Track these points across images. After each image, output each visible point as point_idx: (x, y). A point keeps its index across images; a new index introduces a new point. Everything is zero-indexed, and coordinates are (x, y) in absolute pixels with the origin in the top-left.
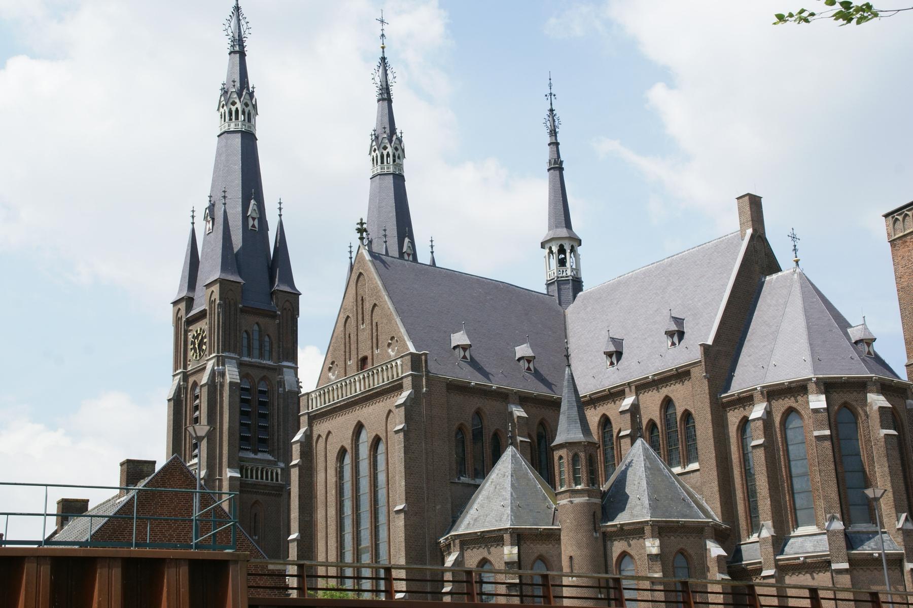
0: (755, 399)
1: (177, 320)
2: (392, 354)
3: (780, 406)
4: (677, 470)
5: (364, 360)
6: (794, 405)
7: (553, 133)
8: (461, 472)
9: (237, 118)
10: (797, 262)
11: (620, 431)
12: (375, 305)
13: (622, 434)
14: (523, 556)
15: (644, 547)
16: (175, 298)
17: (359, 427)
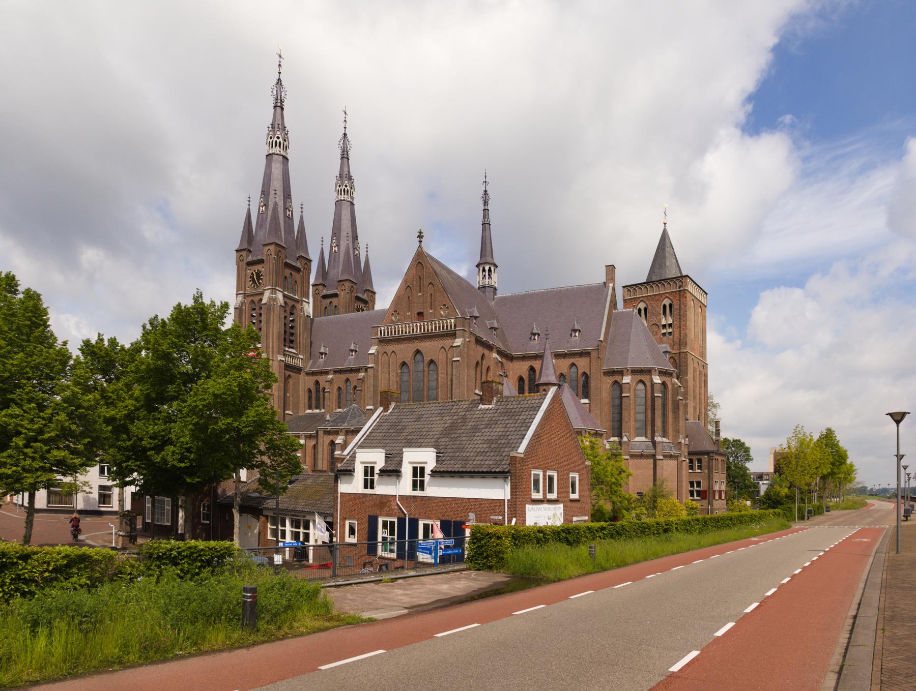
7: (486, 203)
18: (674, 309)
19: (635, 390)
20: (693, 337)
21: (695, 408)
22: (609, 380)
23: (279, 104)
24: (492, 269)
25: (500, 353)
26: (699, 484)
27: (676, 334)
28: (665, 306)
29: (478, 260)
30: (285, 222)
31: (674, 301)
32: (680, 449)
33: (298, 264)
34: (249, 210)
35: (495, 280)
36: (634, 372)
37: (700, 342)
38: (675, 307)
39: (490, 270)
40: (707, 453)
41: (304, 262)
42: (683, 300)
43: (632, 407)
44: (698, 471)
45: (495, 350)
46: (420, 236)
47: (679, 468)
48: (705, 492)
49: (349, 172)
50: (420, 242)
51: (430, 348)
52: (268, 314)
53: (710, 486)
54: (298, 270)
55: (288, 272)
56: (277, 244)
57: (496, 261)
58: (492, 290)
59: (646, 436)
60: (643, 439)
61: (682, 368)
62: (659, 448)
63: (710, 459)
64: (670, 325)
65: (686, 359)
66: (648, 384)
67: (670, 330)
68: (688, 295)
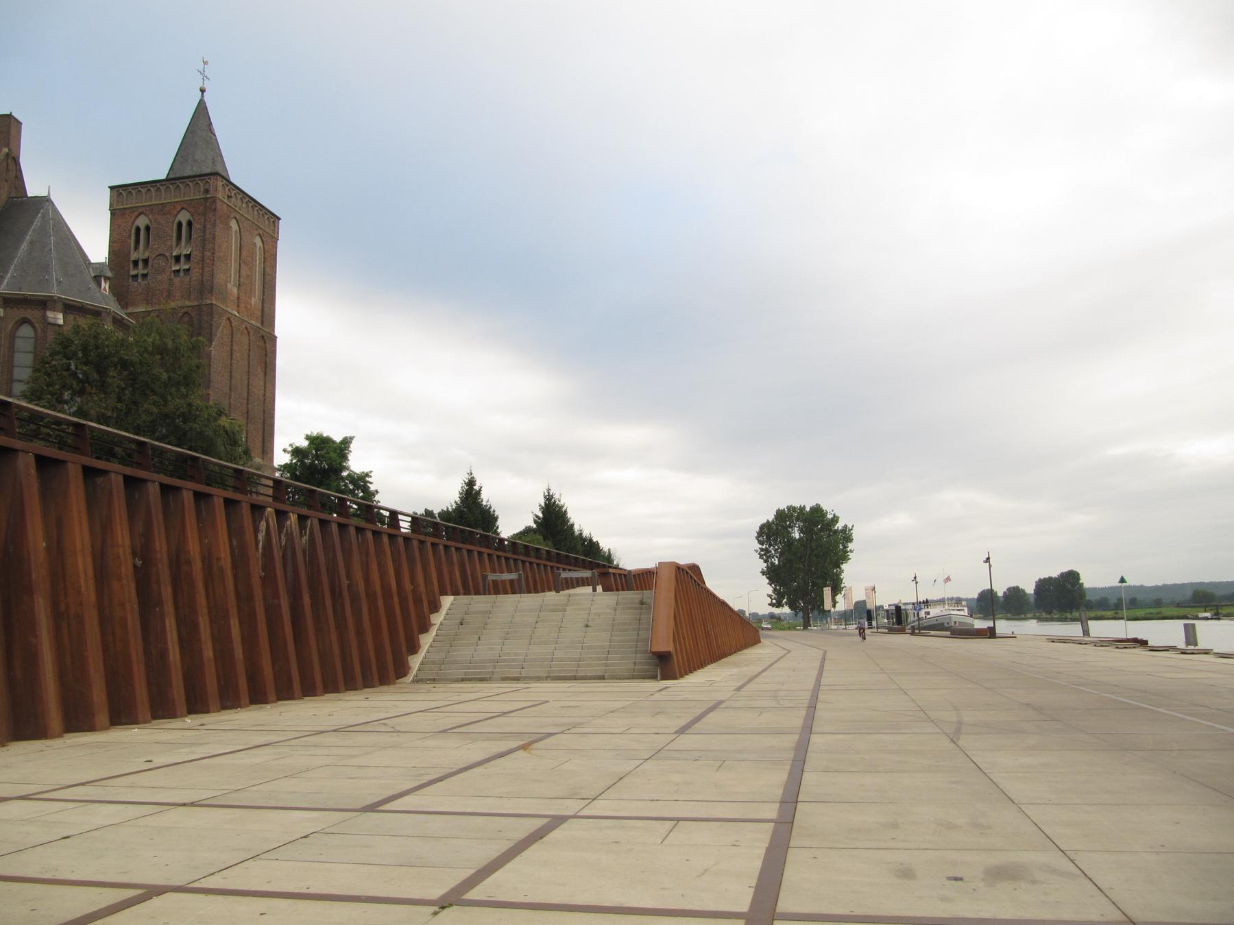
27: (195, 274)
28: (180, 224)
38: (196, 226)
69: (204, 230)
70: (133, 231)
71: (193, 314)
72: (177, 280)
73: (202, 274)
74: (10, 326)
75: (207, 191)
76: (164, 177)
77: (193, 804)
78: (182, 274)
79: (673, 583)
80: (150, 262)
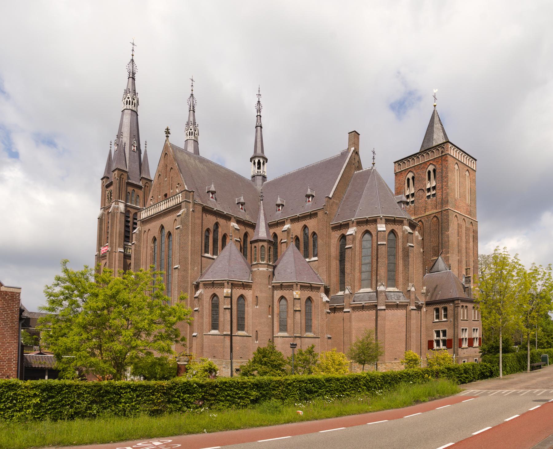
0: (350, 225)
1: (103, 185)
2: (177, 190)
3: (238, 292)
4: (307, 260)
5: (166, 195)
6: (369, 229)
7: (259, 111)
8: (207, 252)
9: (129, 104)
10: (374, 164)
11: (281, 240)
12: (172, 168)
13: (282, 241)
14: (233, 294)
15: (292, 295)
16: (102, 177)
17: (162, 227)
18: (437, 173)
19: (361, 241)
20: (457, 196)
21: (460, 262)
22: (336, 235)
23: (131, 76)
24: (262, 161)
25: (239, 222)
26: (444, 332)
27: (439, 195)
28: (429, 172)
29: (252, 154)
30: (130, 154)
31: (437, 166)
32: (409, 297)
33: (141, 184)
34: (110, 150)
35: (266, 169)
36: (359, 223)
37: (468, 201)
38: (438, 171)
39: (259, 163)
40: (452, 301)
41: (145, 181)
42: (444, 163)
43: (357, 258)
44: (444, 320)
45: (233, 219)
46: (168, 132)
47: (408, 318)
48: (450, 341)
49: (194, 120)
50: (168, 137)
51: (167, 221)
52: (113, 220)
53: (455, 334)
54: (140, 187)
55: (130, 189)
56: (119, 170)
57: (266, 155)
58: (261, 177)
59: (371, 288)
60: (369, 290)
61: (444, 225)
62: (382, 298)
63: (456, 307)
64: (434, 188)
65: (448, 216)
66: (374, 233)
67: (434, 192)
68: (449, 158)
69: (270, 256)
70: (406, 181)
71: (439, 216)
72: (429, 201)
73: (442, 195)
74: (360, 236)
75: (442, 152)
76: (418, 151)
77: (231, 351)
78: (431, 197)
79: (246, 316)
80: (415, 194)
